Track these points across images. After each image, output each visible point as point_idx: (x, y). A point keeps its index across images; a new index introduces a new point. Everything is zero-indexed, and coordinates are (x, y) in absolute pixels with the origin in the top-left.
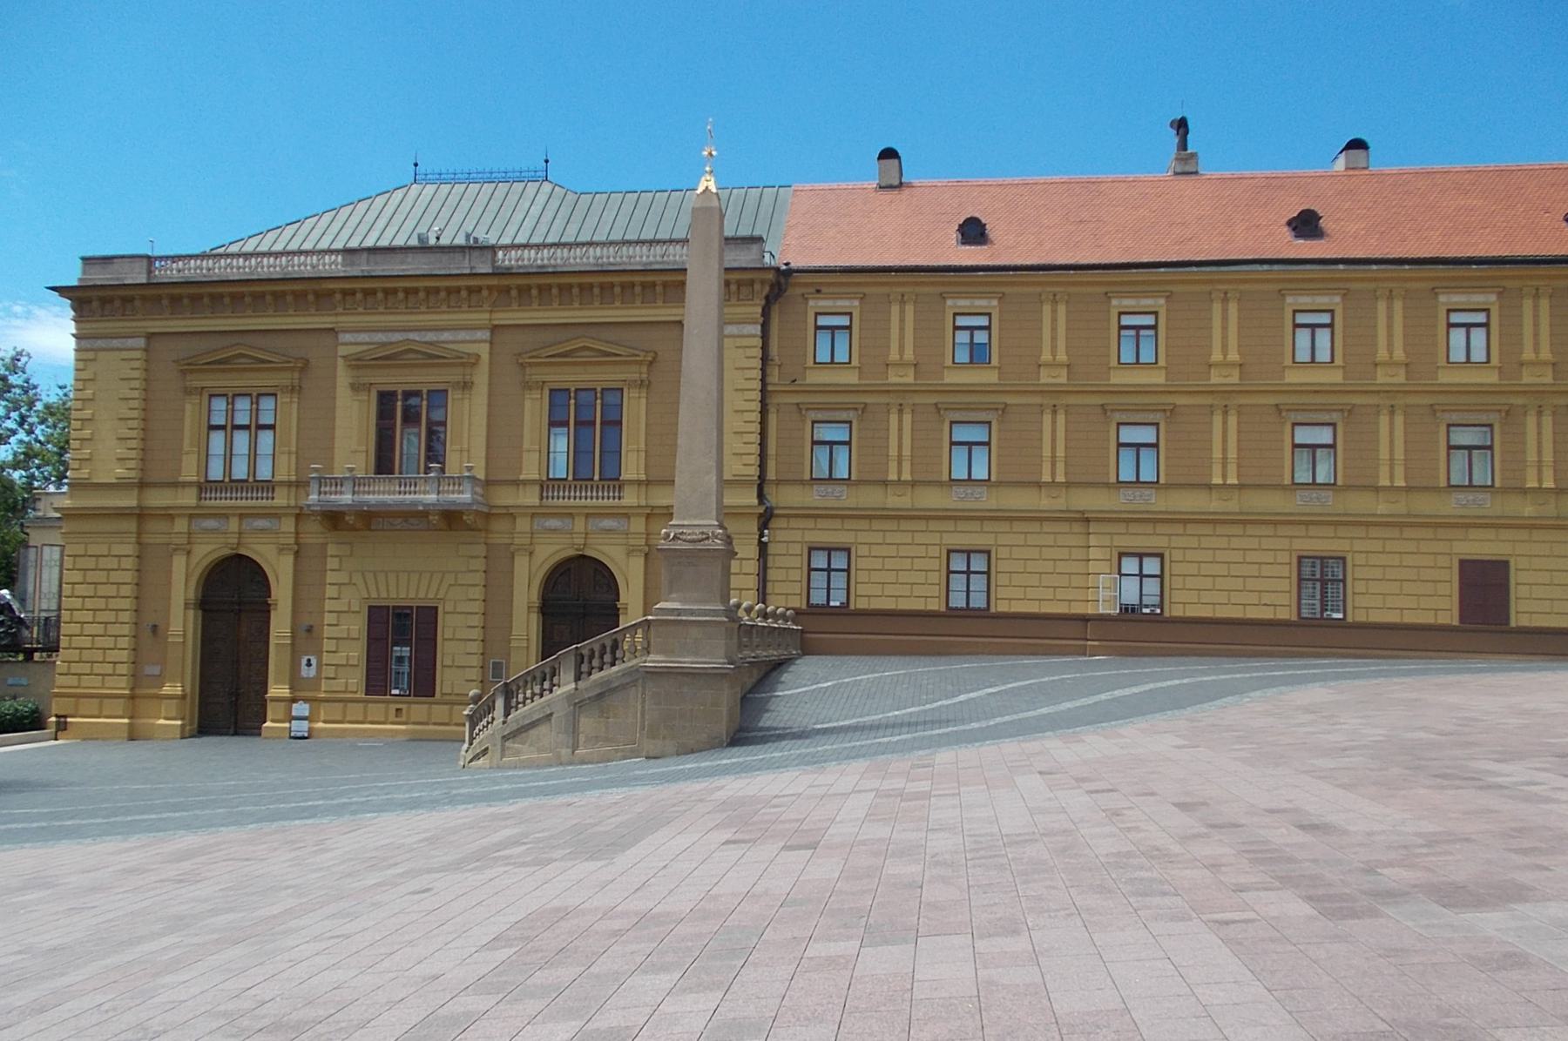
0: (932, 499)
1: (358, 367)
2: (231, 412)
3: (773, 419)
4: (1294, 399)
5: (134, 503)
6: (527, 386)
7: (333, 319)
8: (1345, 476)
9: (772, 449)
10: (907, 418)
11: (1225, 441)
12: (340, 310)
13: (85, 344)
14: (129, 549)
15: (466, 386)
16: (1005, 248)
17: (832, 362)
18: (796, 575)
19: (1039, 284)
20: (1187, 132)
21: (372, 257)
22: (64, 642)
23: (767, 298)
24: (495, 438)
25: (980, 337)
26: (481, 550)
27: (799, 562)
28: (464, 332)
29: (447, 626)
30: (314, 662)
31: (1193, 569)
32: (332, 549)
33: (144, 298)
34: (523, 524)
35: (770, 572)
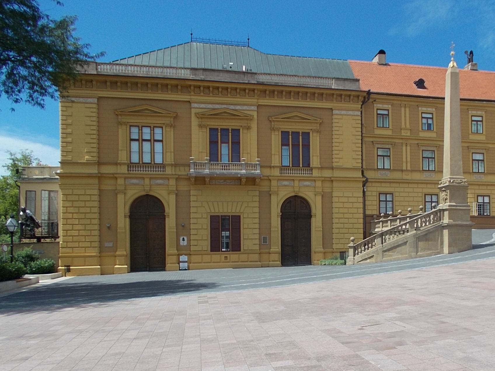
0: (417, 176)
1: (202, 118)
2: (152, 134)
4: (423, 142)
5: (97, 172)
6: (273, 129)
7: (189, 97)
8: (438, 168)
10: (409, 148)
14: (96, 192)
15: (249, 128)
18: (375, 203)
19: (401, 101)
20: (473, 56)
21: (204, 73)
24: (258, 151)
25: (430, 121)
26: (257, 193)
27: (376, 198)
28: (247, 106)
29: (245, 223)
30: (186, 239)
31: (402, 199)
32: (192, 192)
33: (97, 81)
34: (120, 181)
35: (366, 202)
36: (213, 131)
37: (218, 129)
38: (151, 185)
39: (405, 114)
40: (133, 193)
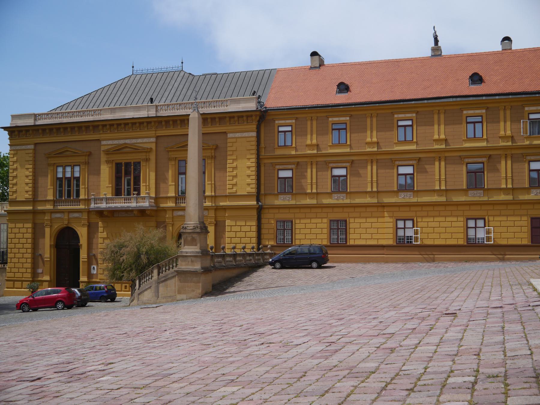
3: (262, 169)
6: (170, 159)
9: (262, 181)
11: (440, 171)
12: (101, 132)
13: (13, 148)
14: (30, 225)
15: (147, 160)
16: (356, 96)
17: (405, 140)
22: (9, 260)
23: (259, 121)
30: (95, 268)
32: (100, 224)
34: (168, 215)
36: (118, 166)
37: (131, 163)
38: (69, 219)
39: (312, 127)
40: (57, 226)
